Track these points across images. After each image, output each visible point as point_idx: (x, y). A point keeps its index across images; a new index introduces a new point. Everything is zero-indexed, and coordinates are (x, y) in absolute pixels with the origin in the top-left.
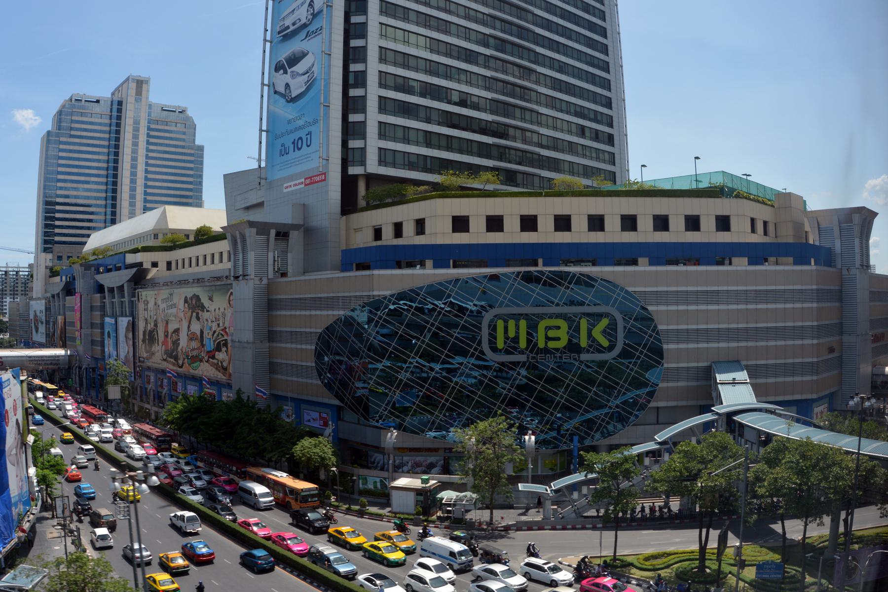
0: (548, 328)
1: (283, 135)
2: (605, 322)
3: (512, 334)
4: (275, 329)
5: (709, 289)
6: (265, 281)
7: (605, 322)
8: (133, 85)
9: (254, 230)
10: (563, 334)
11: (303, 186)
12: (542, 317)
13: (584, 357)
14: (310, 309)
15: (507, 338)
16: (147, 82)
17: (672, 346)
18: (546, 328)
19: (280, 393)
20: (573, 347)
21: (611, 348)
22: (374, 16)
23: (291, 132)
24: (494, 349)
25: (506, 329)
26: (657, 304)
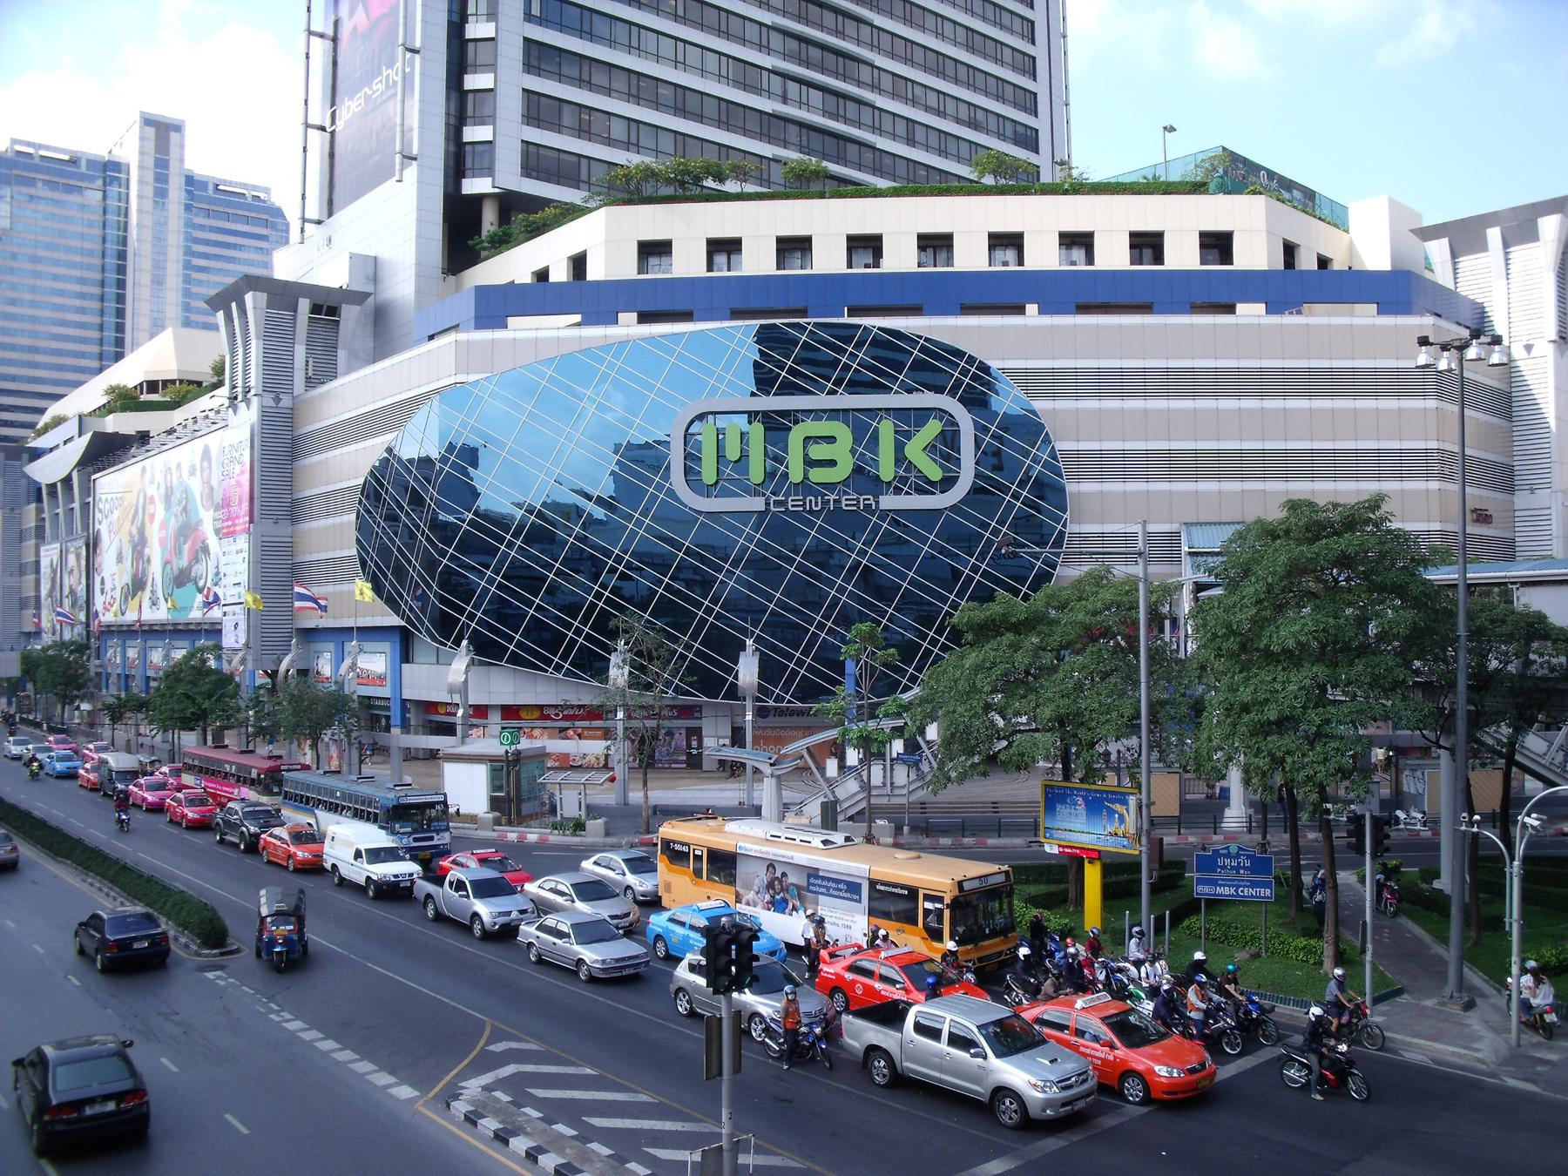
0: (807, 440)
2: (933, 428)
3: (733, 453)
7: (933, 428)
8: (151, 132)
12: (793, 416)
13: (888, 502)
15: (720, 457)
16: (178, 128)
17: (1087, 487)
18: (807, 440)
20: (863, 477)
21: (948, 483)
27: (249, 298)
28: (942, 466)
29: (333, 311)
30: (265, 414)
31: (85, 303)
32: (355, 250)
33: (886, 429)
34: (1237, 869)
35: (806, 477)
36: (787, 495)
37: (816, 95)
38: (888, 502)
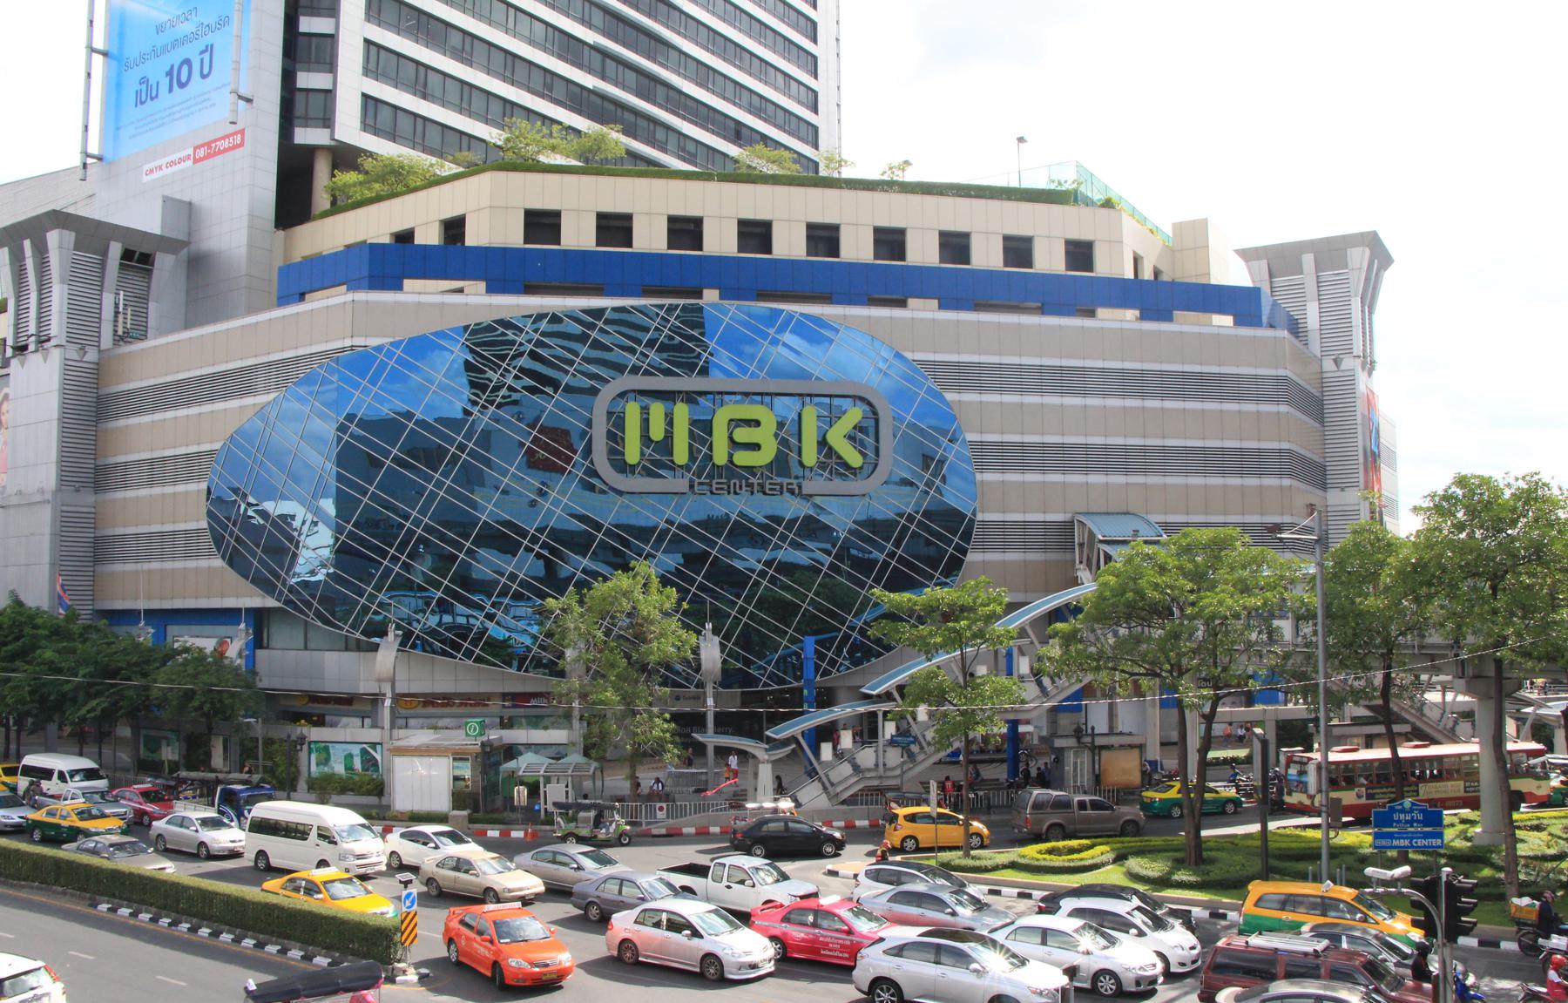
1: (144, 58)
2: (854, 415)
3: (657, 433)
4: (110, 532)
5: (1065, 362)
9: (70, 236)
10: (766, 436)
11: (190, 163)
14: (200, 402)
15: (646, 438)
19: (119, 605)
22: (353, 26)
23: (165, 49)
24: (622, 467)
25: (645, 423)
26: (960, 389)
30: (67, 367)
32: (168, 193)
35: (731, 461)
37: (631, 75)
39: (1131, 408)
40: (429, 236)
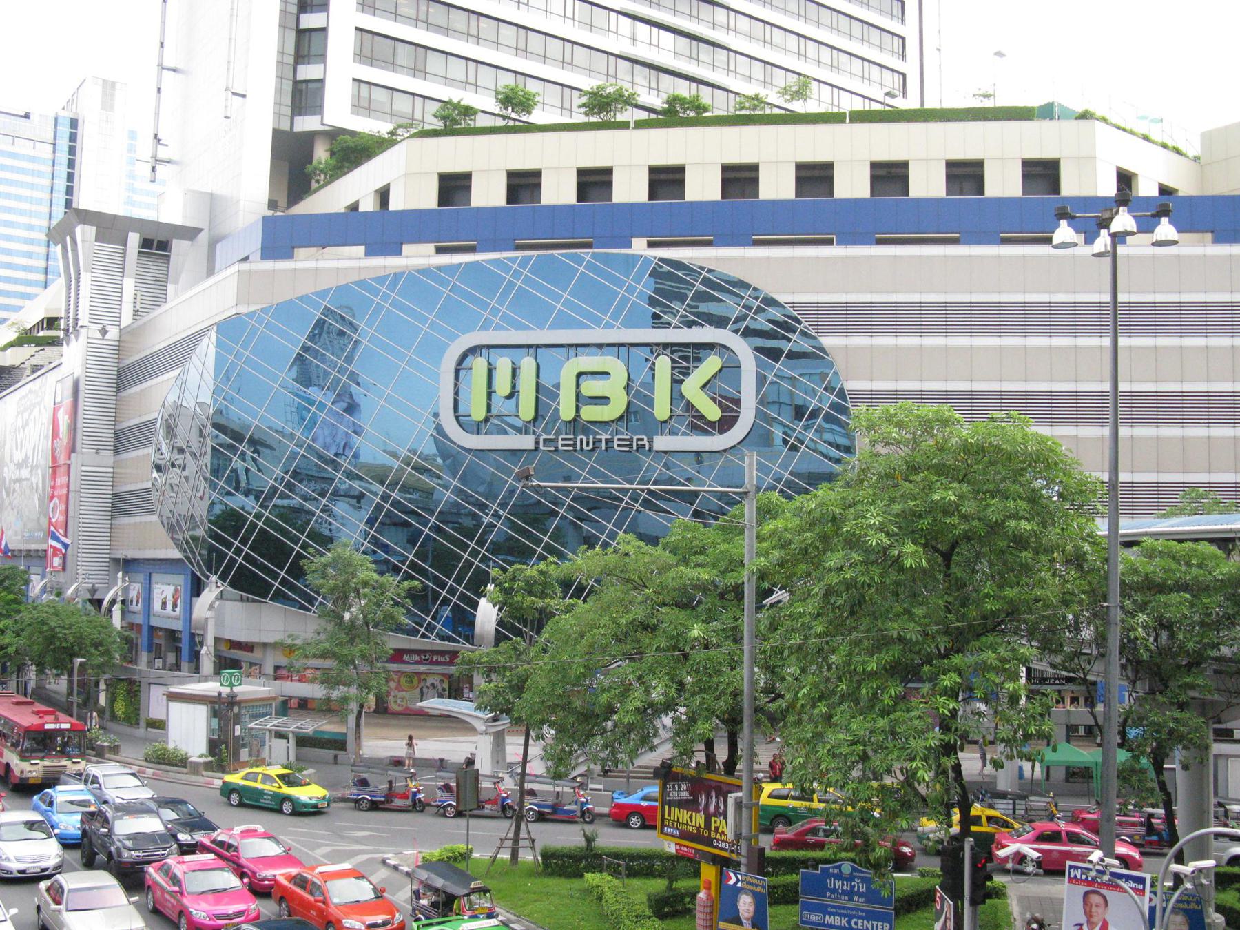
3: (502, 385)
6: (113, 333)
7: (712, 364)
9: (91, 231)
10: (615, 389)
13: (662, 442)
19: (131, 554)
21: (725, 424)
22: (342, 18)
26: (847, 332)
27: (79, 230)
28: (720, 405)
29: (164, 246)
31: (32, 249)
33: (664, 364)
34: (850, 894)
36: (558, 433)
38: (662, 442)
39: (1059, 348)
40: (368, 205)
